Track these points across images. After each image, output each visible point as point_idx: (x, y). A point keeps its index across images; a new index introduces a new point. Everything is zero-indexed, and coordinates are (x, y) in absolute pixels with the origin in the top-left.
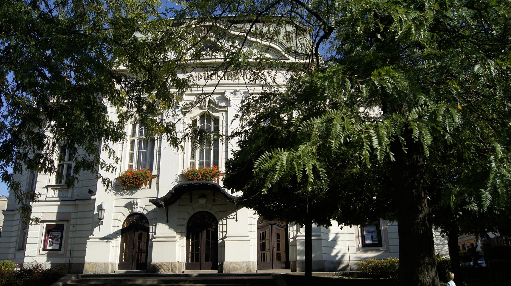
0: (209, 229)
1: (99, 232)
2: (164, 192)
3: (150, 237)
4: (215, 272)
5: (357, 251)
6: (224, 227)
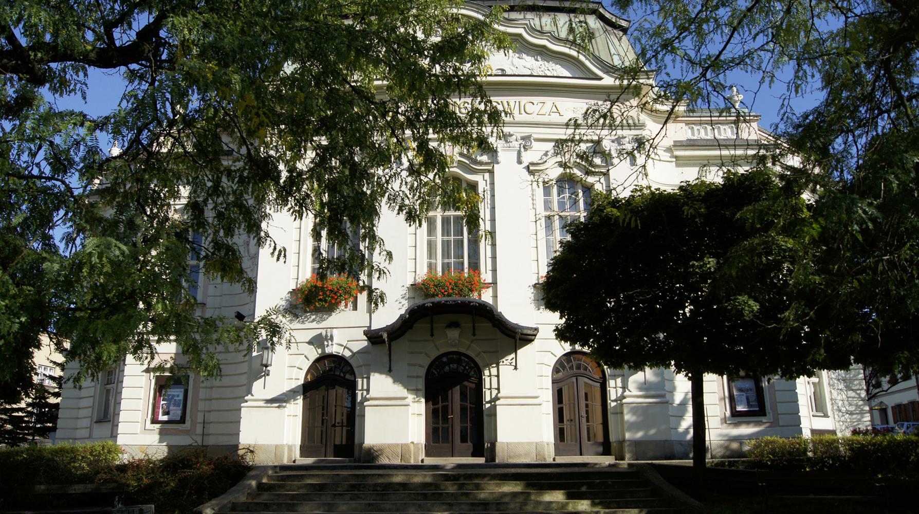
0: (466, 383)
1: (261, 389)
2: (389, 314)
3: (359, 398)
4: (481, 460)
5: (722, 424)
6: (494, 380)
